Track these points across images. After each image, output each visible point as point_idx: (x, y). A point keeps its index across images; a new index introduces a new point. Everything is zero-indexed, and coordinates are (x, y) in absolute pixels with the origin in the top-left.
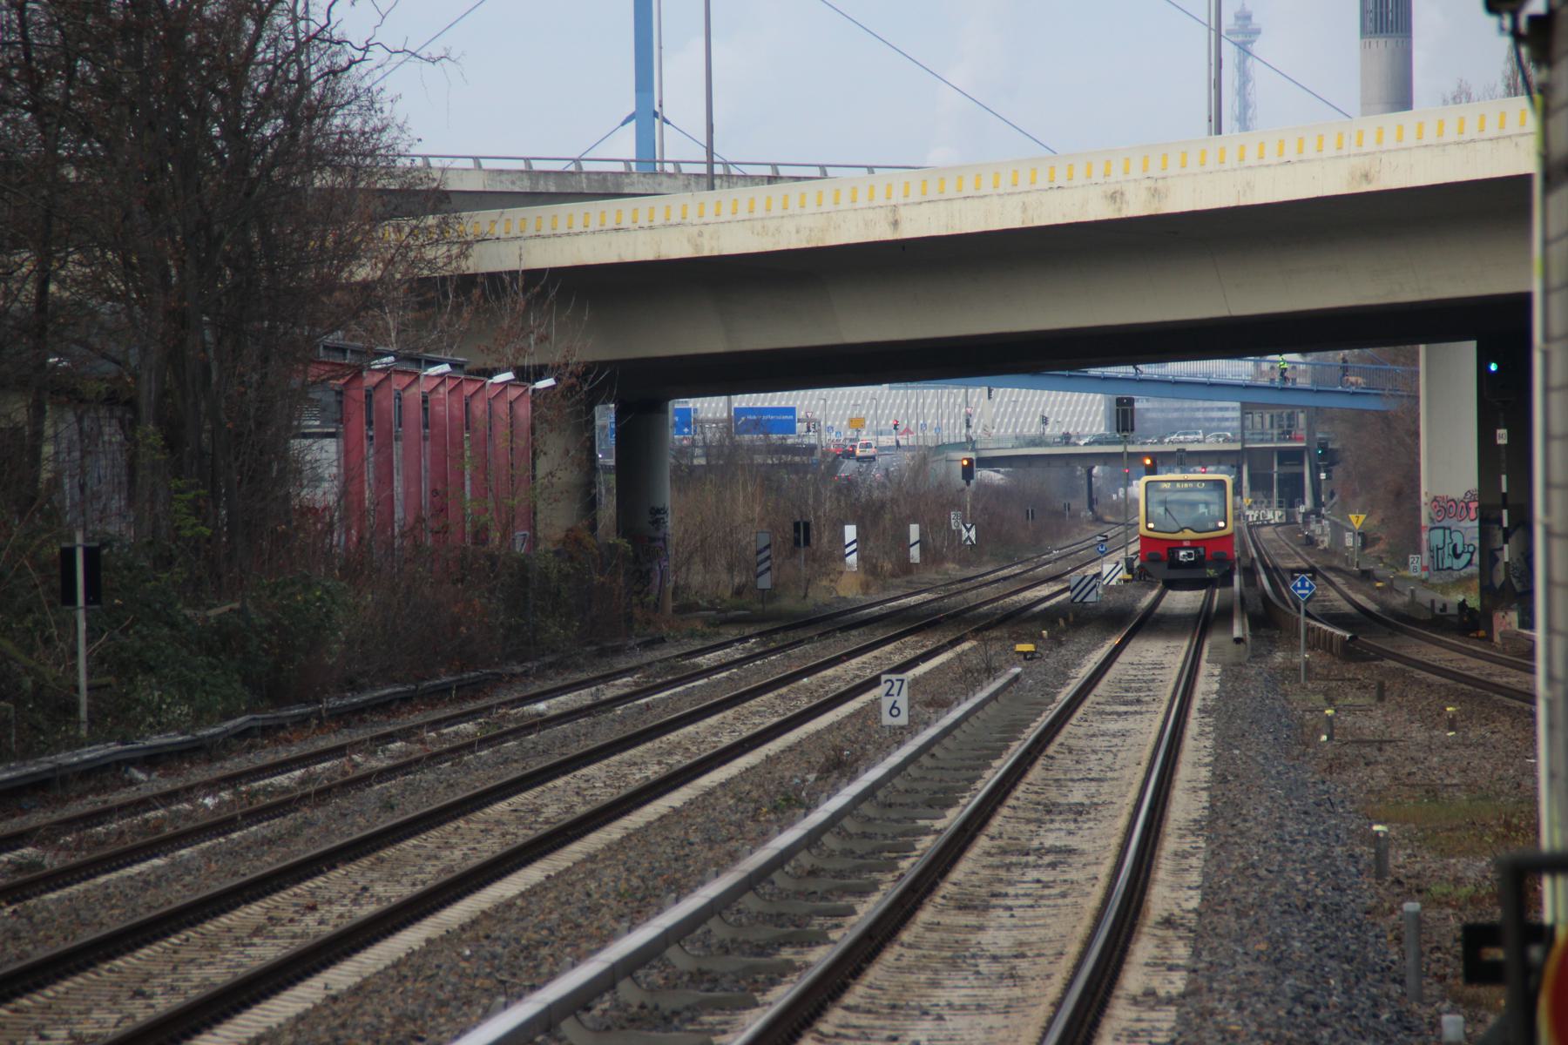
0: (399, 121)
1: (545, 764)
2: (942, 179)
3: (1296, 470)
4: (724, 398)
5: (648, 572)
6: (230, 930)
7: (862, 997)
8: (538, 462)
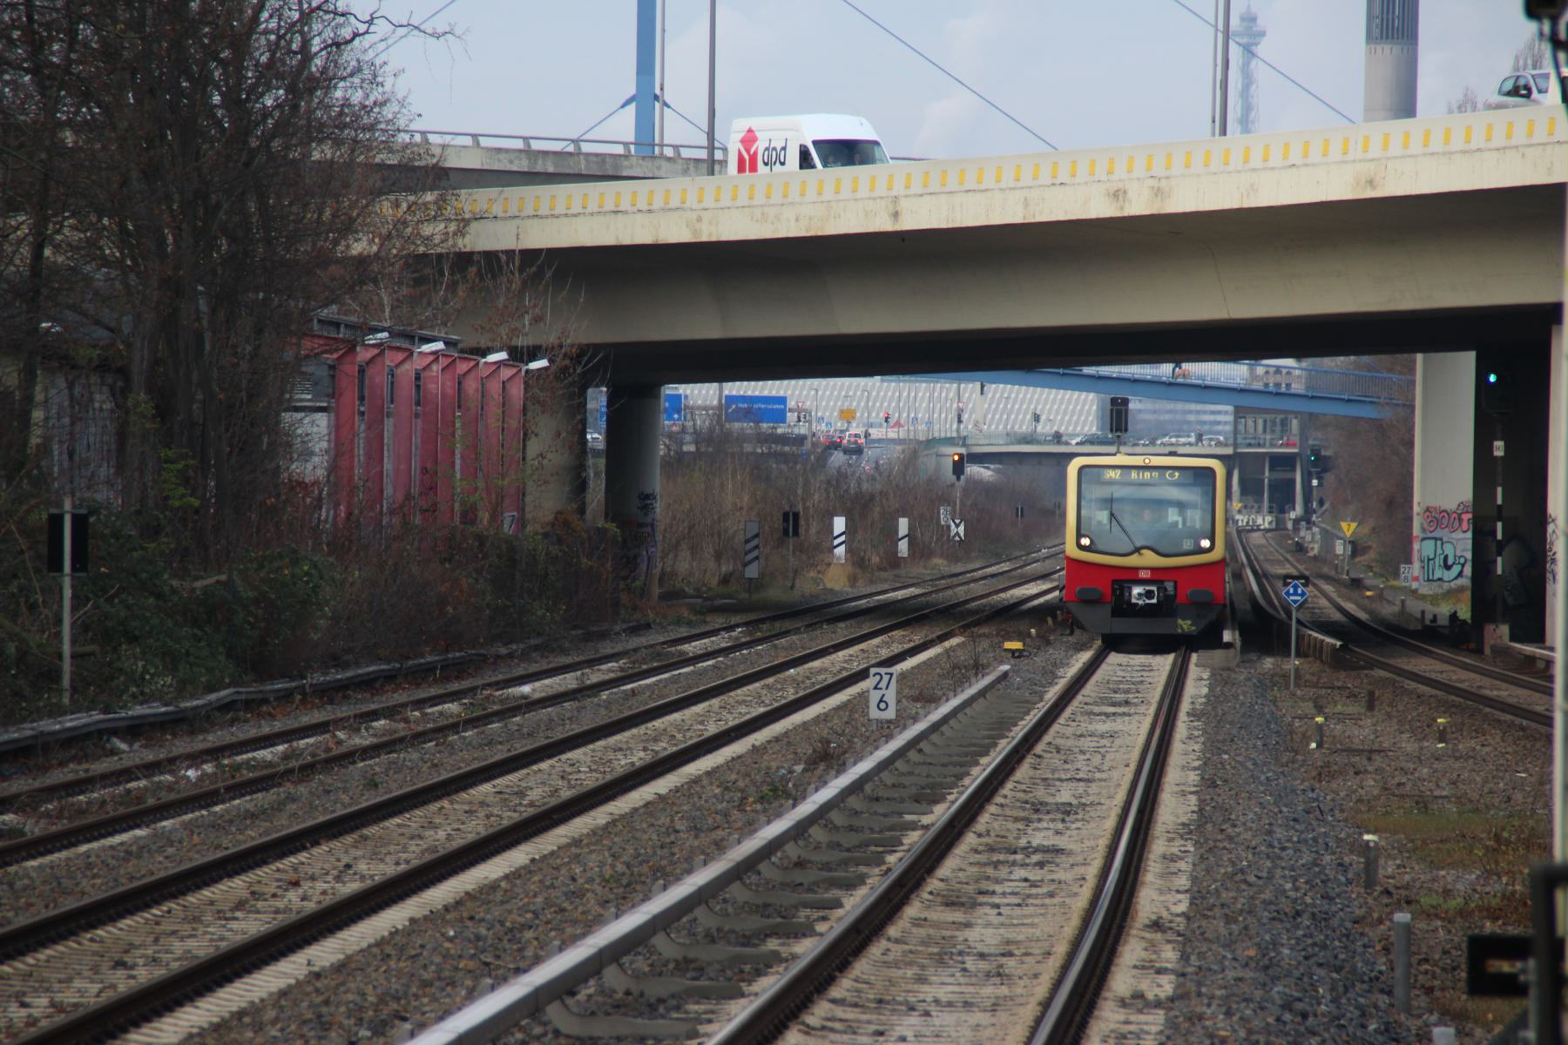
0: (400, 96)
1: (529, 747)
3: (1288, 475)
4: (715, 385)
5: (636, 557)
6: (212, 903)
7: (848, 990)
8: (528, 443)
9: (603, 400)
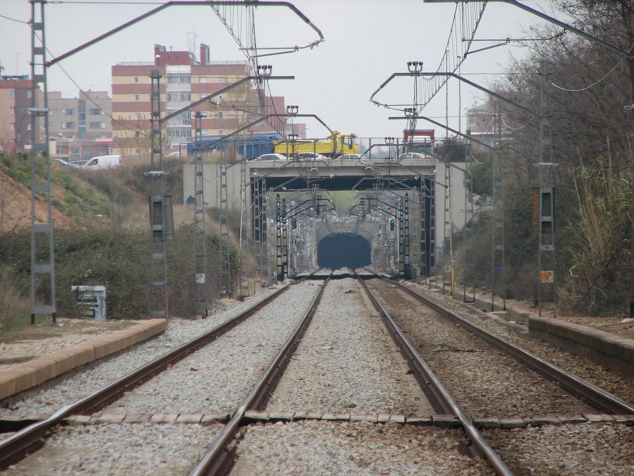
2: (72, 249)
9: (132, 119)
